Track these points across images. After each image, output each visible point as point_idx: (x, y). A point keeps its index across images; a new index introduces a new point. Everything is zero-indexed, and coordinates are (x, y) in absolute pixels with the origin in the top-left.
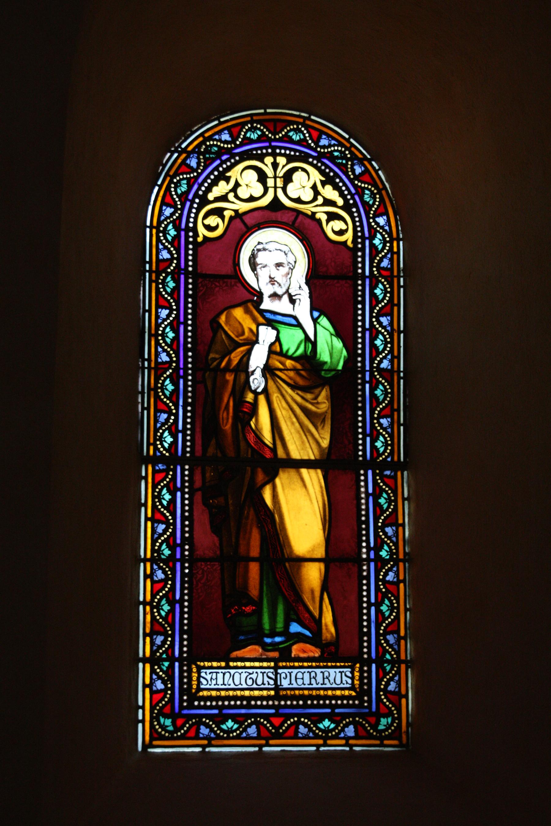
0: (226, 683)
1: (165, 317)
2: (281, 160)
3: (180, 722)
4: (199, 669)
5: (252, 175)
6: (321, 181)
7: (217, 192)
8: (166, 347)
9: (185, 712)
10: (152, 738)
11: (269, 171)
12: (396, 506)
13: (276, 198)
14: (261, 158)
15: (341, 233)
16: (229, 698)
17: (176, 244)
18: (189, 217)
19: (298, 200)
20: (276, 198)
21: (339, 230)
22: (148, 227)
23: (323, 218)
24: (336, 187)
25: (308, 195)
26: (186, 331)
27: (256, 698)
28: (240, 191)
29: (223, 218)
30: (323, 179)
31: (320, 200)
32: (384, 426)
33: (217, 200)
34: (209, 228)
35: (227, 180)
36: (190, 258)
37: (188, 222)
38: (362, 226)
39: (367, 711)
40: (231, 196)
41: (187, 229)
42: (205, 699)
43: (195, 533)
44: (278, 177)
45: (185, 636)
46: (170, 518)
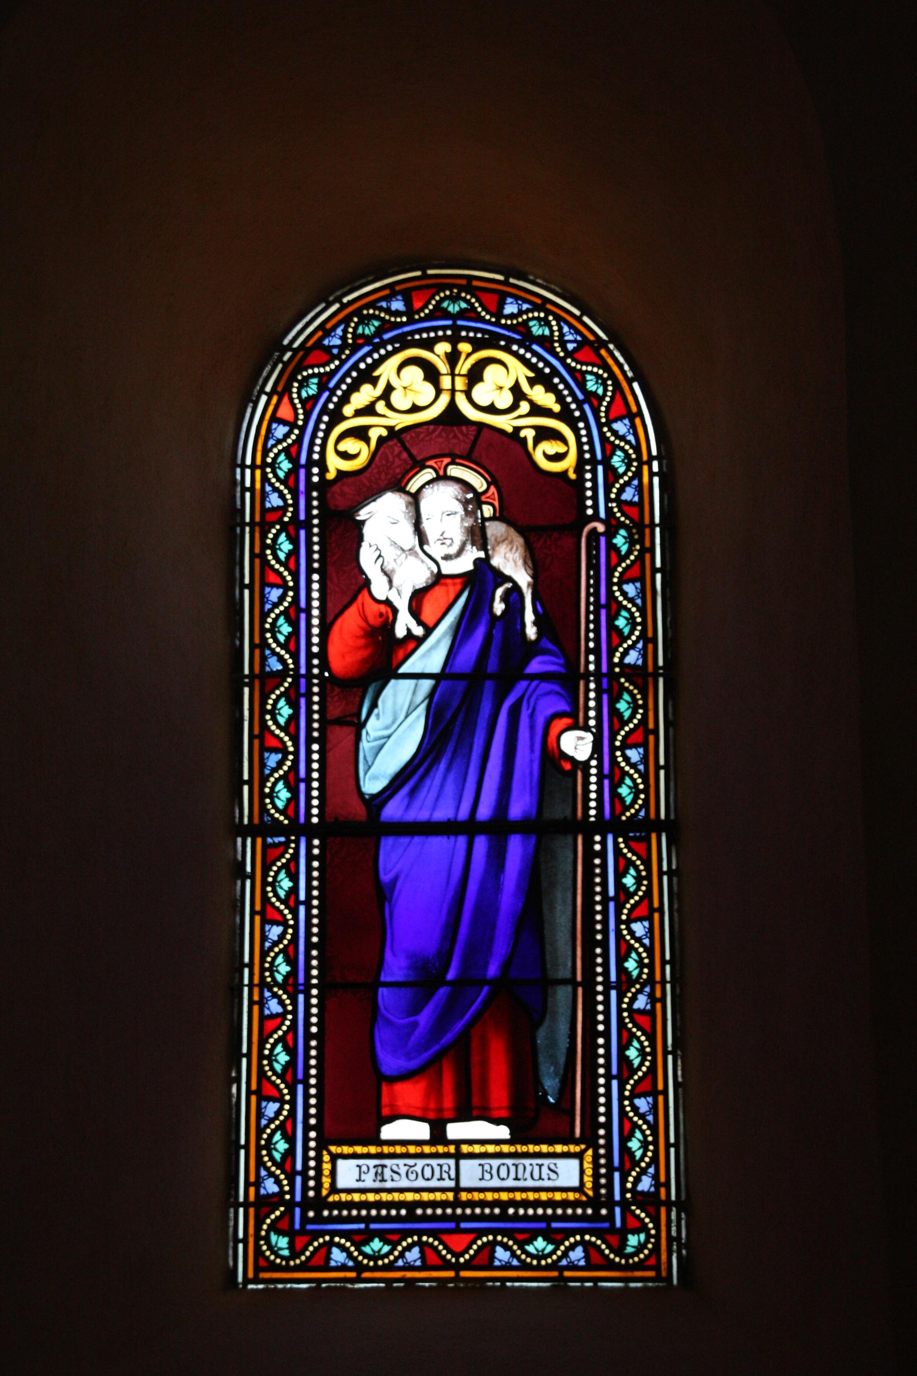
0: (520, 1176)
1: (276, 938)
2: (465, 347)
3: (300, 1241)
4: (334, 1158)
5: (414, 373)
6: (528, 378)
7: (360, 399)
8: (273, 1169)
9: (310, 1227)
10: (257, 1270)
11: (443, 368)
12: (654, 1062)
13: (452, 404)
14: (429, 345)
15: (558, 457)
16: (379, 1205)
17: (292, 565)
18: (312, 444)
19: (491, 409)
20: (452, 404)
21: (555, 457)
22: (248, 524)
23: (529, 434)
24: (550, 388)
25: (505, 400)
26: (309, 916)
27: (424, 1205)
28: (395, 398)
29: (367, 440)
30: (531, 375)
31: (525, 407)
32: (642, 1111)
33: (358, 413)
34: (345, 456)
35: (374, 381)
36: (316, 707)
37: (310, 451)
38: (591, 442)
39: (606, 1225)
40: (381, 407)
41: (310, 463)
42: (340, 1205)
43: (327, 781)
44: (459, 375)
45: (315, 494)
46: (286, 1091)
